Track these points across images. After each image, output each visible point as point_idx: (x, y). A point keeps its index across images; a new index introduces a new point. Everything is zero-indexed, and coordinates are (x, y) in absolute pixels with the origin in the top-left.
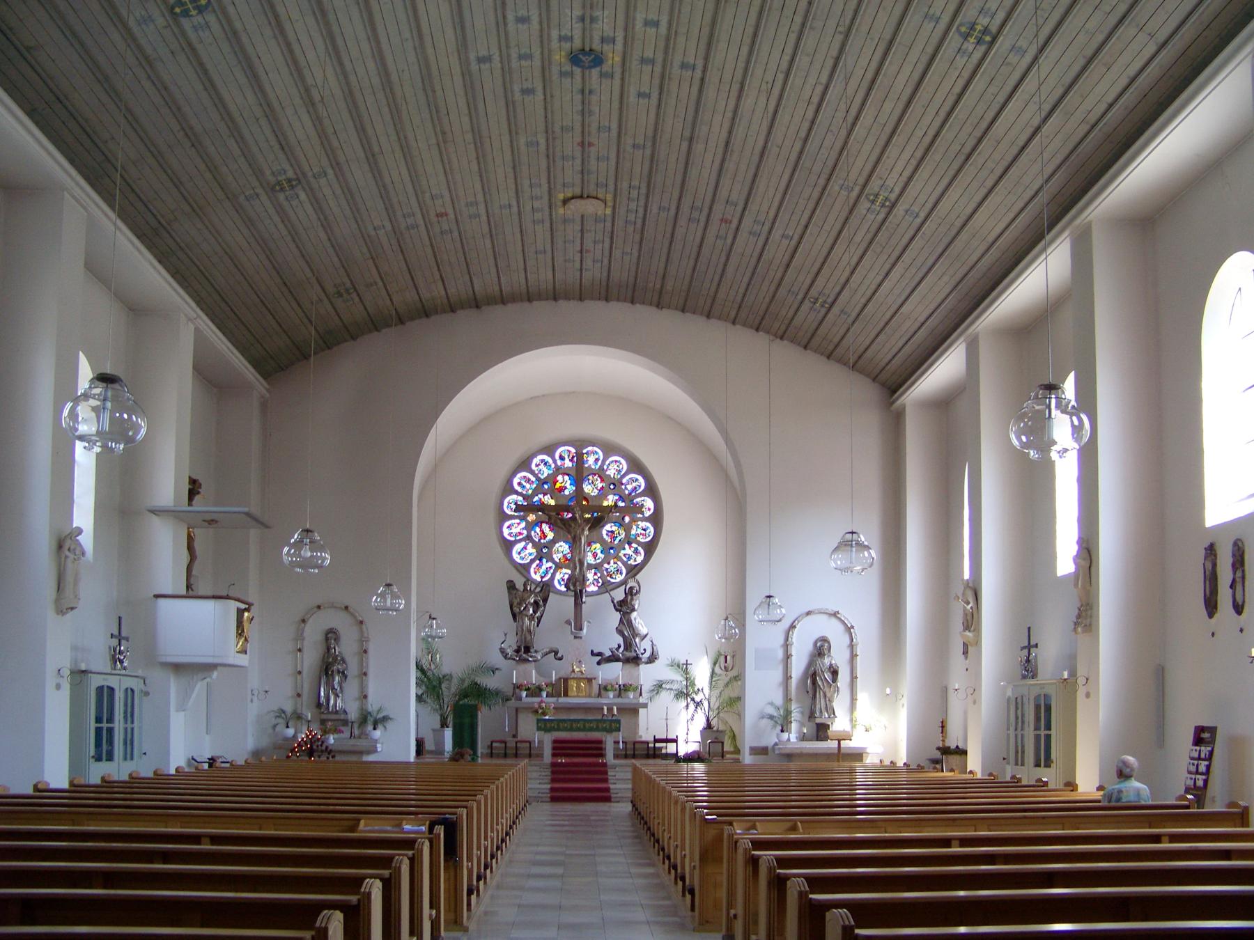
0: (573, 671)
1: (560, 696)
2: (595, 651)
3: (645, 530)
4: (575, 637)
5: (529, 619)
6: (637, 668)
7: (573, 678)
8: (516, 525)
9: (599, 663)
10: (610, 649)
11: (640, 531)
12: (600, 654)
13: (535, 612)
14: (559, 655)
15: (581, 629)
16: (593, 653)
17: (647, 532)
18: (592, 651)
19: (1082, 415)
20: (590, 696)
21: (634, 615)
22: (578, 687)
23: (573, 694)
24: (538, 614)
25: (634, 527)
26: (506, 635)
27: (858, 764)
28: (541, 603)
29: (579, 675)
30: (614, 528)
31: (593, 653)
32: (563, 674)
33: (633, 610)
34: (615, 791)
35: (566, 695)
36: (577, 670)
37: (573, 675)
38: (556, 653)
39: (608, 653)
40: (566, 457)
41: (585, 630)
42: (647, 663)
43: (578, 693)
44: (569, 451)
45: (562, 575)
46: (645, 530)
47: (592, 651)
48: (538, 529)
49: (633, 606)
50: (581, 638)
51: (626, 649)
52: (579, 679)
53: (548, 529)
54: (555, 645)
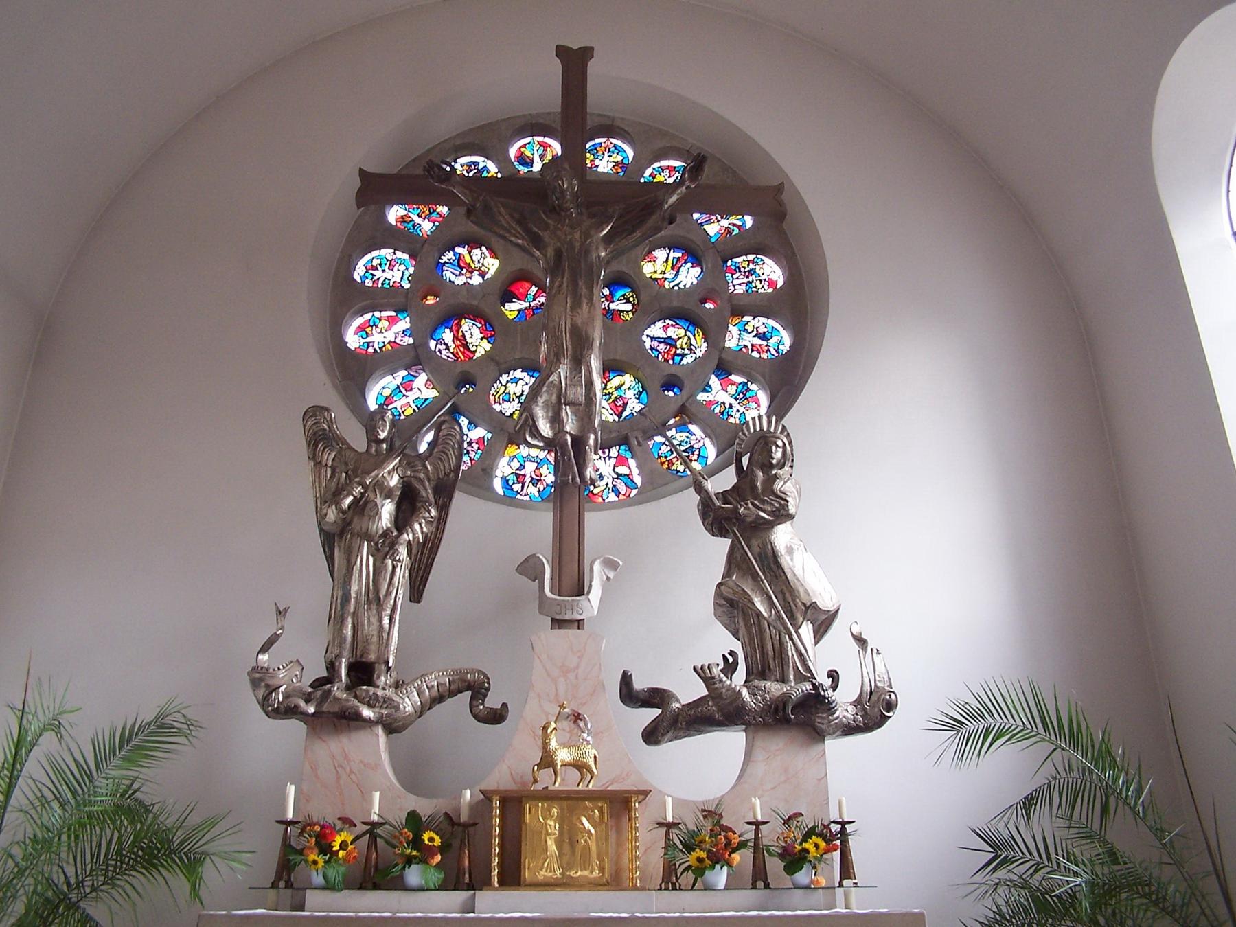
0: (547, 761)
1: (478, 882)
2: (639, 684)
3: (763, 337)
4: (558, 623)
5: (376, 551)
6: (815, 750)
7: (549, 796)
8: (385, 324)
9: (652, 735)
10: (701, 672)
11: (749, 340)
12: (655, 697)
13: (402, 521)
14: (493, 701)
15: (580, 590)
16: (630, 695)
17: (773, 341)
18: (626, 679)
19: (369, 827)
20: (614, 881)
21: (782, 536)
22: (569, 838)
23: (543, 875)
24: (419, 529)
25: (733, 330)
26: (281, 613)
27: (334, 693)
28: (427, 492)
29: (568, 781)
30: (673, 332)
31: (630, 695)
32: (500, 778)
33: (782, 514)
34: (533, 810)
35: (512, 878)
36: (563, 756)
37: (546, 779)
38: (478, 690)
39: (689, 690)
40: (536, 158)
41: (595, 595)
42: (850, 730)
43: (565, 868)
44: (545, 146)
45: (515, 465)
46: (763, 337)
47: (626, 679)
48: (448, 336)
49: (782, 499)
50: (579, 623)
51: (758, 672)
52: (572, 800)
53: (477, 334)
54: (472, 659)
